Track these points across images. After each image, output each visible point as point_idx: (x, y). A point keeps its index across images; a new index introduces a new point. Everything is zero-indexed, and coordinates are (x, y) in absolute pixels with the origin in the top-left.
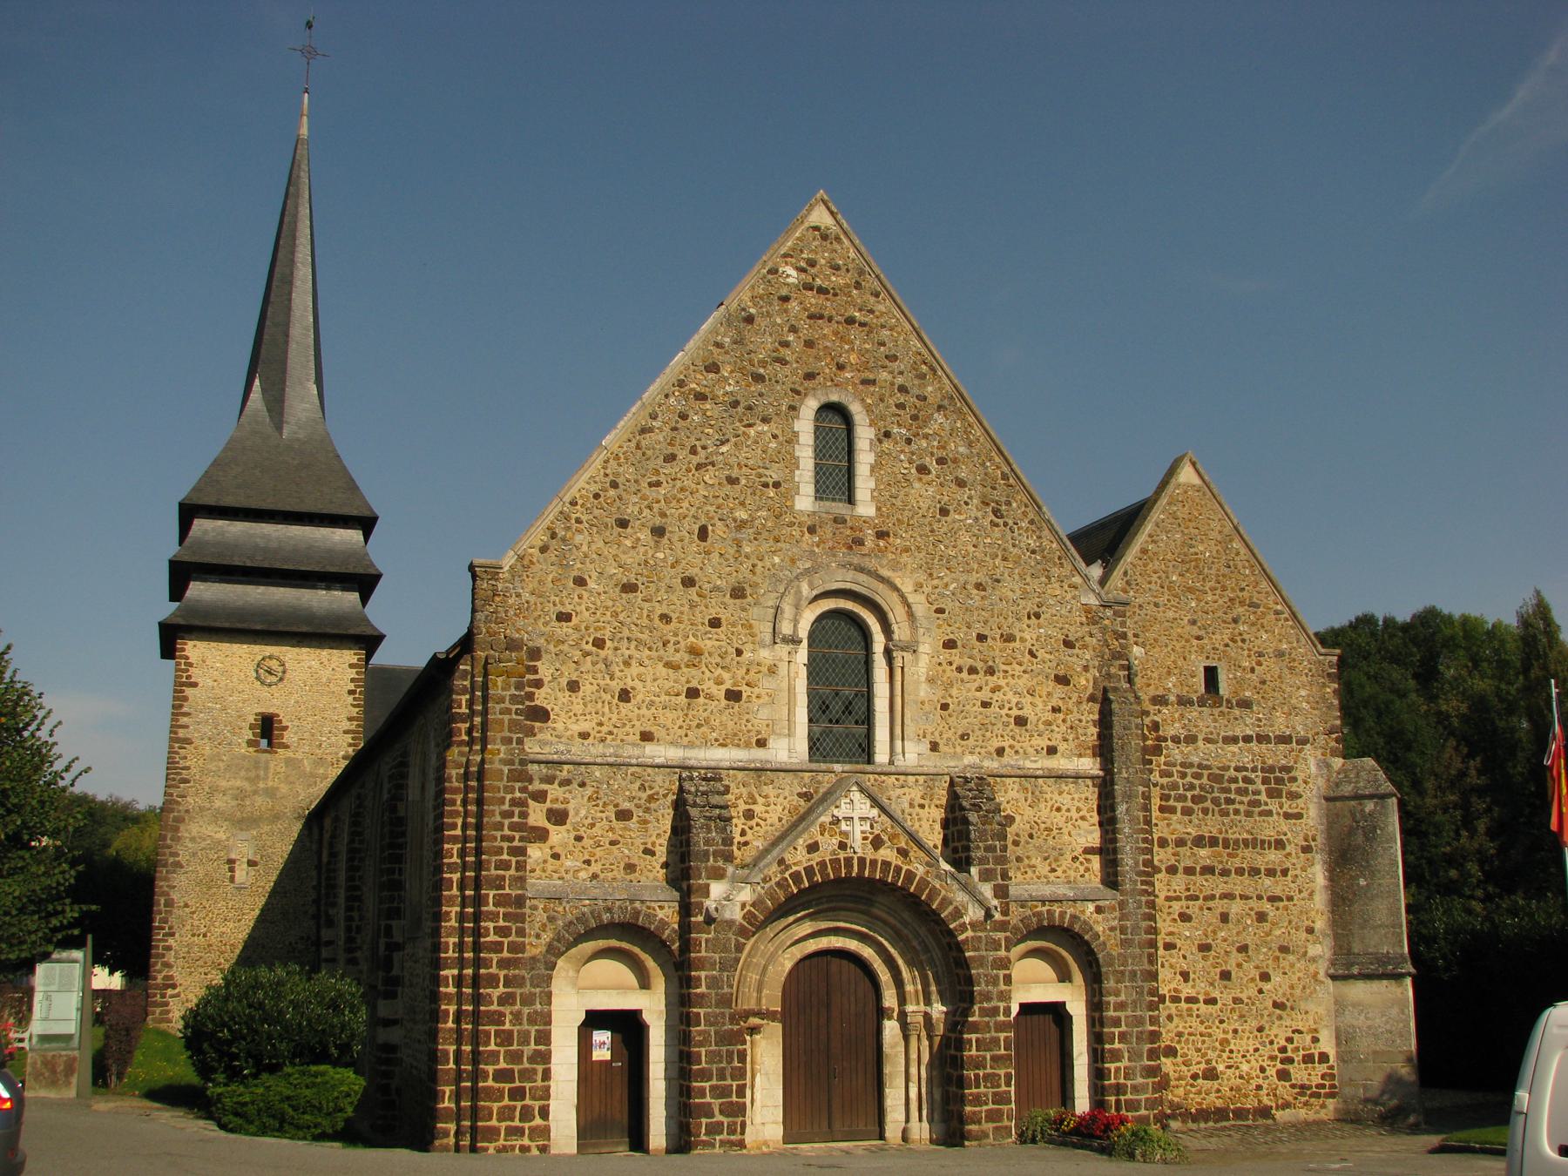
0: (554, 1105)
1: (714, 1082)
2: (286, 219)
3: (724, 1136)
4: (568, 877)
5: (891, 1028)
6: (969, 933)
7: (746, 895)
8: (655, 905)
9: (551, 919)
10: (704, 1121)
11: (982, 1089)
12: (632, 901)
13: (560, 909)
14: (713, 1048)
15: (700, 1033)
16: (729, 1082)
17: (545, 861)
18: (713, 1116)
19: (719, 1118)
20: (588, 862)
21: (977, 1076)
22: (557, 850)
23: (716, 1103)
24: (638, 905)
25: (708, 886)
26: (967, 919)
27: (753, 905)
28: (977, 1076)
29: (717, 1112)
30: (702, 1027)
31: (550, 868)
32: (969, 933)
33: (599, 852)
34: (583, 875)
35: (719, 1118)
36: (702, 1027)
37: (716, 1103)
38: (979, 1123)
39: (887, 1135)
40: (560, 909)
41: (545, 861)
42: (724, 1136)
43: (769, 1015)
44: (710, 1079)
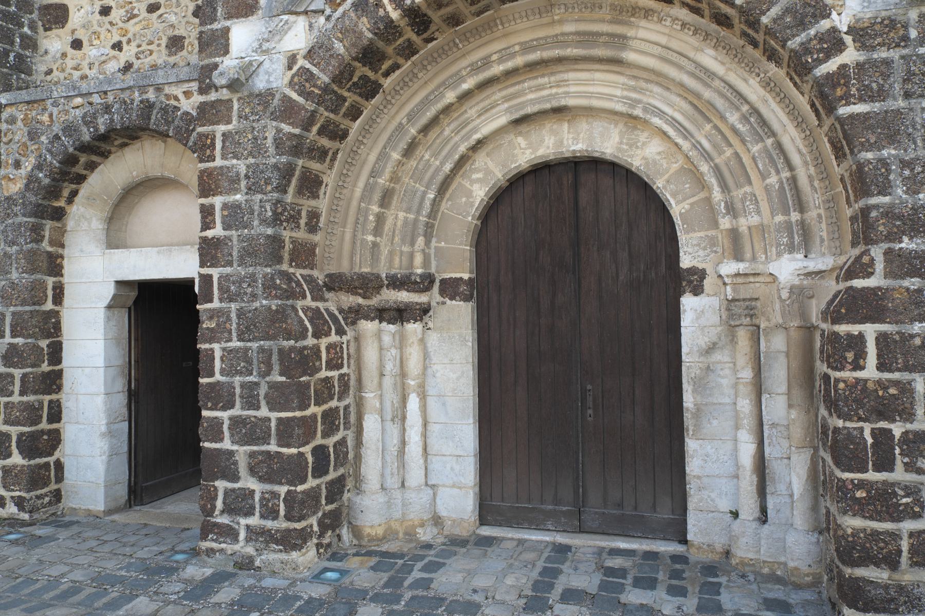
0: (70, 430)
1: (237, 411)
2: (714, 111)
3: (254, 521)
4: (91, 73)
5: (697, 315)
6: (850, 55)
7: (298, 36)
8: (178, 91)
9: (33, 136)
10: (221, 485)
11: (899, 474)
12: (143, 89)
13: (45, 118)
14: (235, 344)
15: (213, 314)
16: (264, 412)
17: (64, 55)
18: (235, 478)
19: (250, 483)
20: (118, 46)
21: (883, 437)
22: (81, 34)
23: (242, 452)
24: (151, 95)
25: (227, 30)
26: (841, 21)
27: (310, 54)
28: (883, 437)
29: (243, 470)
30: (216, 304)
31: (70, 63)
32: (850, 55)
33: (133, 27)
34: (113, 67)
35: (250, 483)
36: (216, 304)
37: (242, 452)
38: (892, 562)
39: (689, 537)
40: (45, 118)
41: (64, 55)
42: (254, 521)
43: (450, 288)
44: (230, 405)
